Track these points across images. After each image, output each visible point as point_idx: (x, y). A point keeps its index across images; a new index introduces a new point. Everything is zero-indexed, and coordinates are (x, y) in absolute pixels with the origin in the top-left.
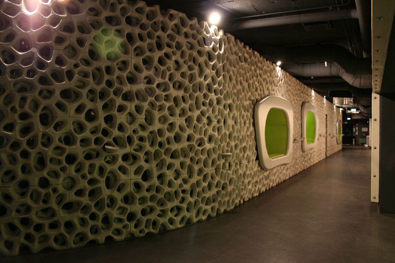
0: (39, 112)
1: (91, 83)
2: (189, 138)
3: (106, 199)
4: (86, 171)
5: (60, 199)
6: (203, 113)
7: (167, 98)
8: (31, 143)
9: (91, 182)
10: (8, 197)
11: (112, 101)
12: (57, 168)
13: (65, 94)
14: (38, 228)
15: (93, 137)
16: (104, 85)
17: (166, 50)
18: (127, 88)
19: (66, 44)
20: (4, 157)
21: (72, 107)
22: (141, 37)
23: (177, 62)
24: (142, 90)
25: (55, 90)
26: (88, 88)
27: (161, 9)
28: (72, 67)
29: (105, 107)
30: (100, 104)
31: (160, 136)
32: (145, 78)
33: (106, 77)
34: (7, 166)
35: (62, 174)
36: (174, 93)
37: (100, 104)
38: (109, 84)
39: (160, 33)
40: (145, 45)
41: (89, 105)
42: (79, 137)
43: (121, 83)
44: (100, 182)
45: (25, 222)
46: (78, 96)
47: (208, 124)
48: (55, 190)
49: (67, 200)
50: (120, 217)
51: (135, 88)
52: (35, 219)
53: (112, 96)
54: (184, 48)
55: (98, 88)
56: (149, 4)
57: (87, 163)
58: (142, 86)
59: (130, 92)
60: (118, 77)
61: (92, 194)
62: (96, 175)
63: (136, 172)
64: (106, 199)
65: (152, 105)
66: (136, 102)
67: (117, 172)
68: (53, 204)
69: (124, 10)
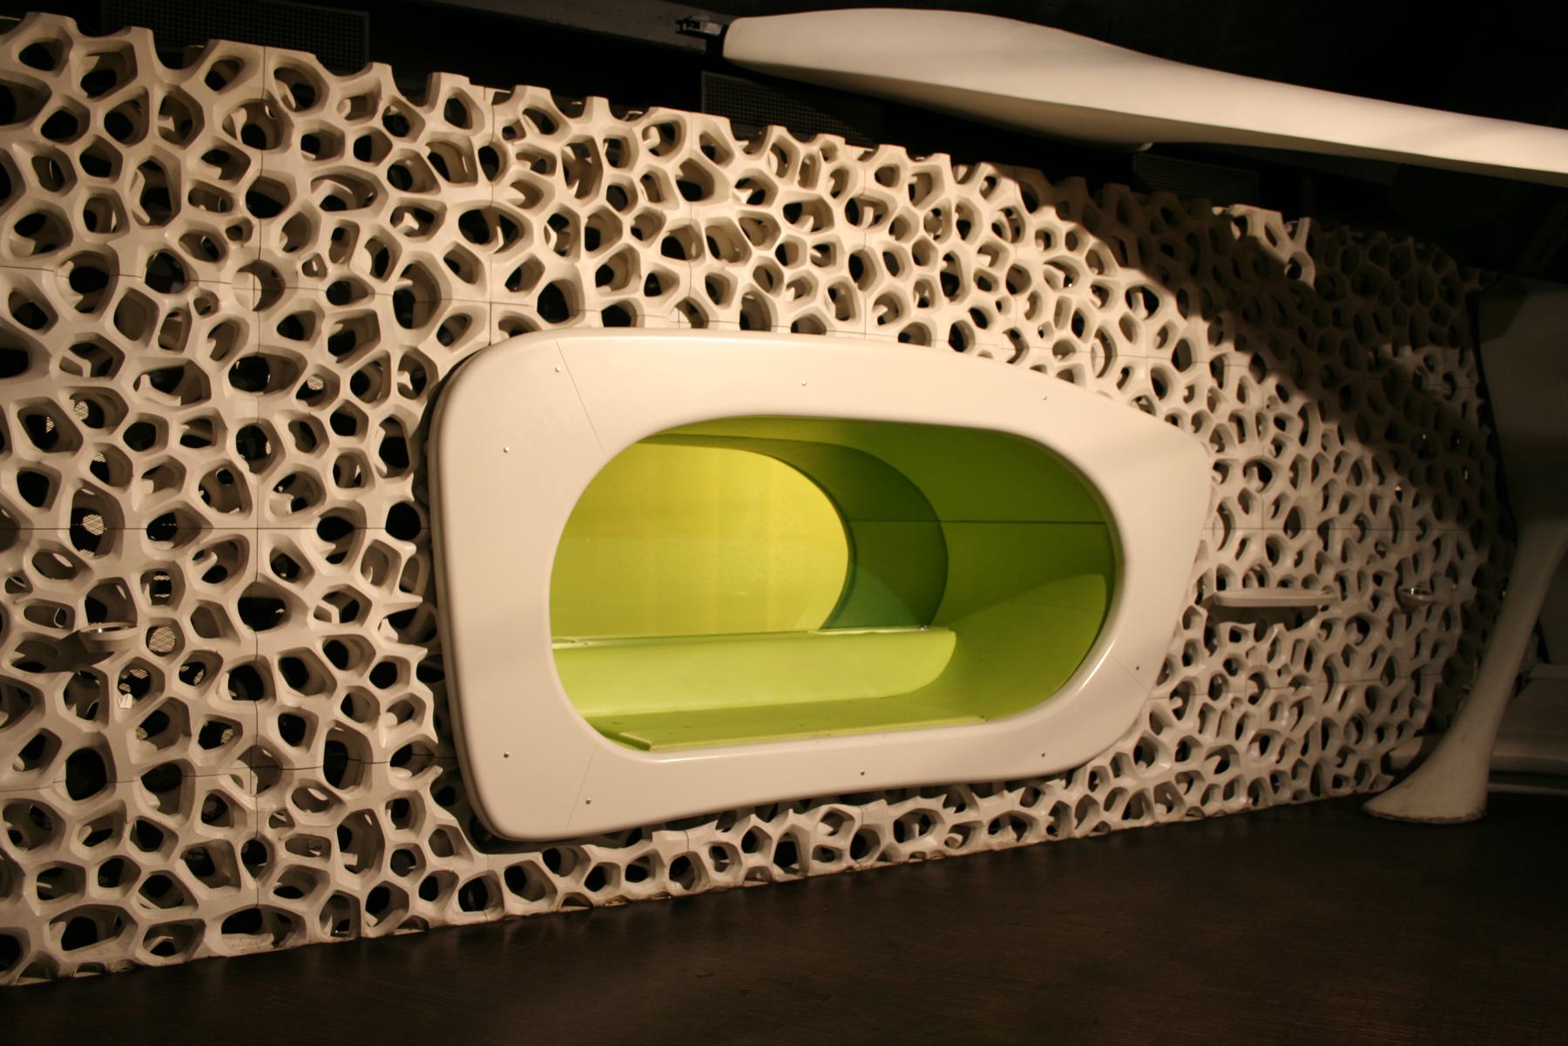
0: (395, 281)
1: (560, 193)
2: (1184, 750)
3: (395, 364)
4: (322, 244)
5: (226, 335)
6: (1231, 666)
7: (826, 252)
8: (125, 125)
9: (342, 292)
10: (34, 311)
11: (627, 257)
12: (219, 223)
13: (476, 224)
14: (146, 434)
15: (352, 133)
16: (600, 200)
17: (975, 296)
18: (678, 212)
19: (678, 295)
20: (23, 157)
21: (497, 264)
22: (893, 263)
23: (1014, 335)
24: (730, 223)
25: (444, 208)
26: (550, 210)
27: (955, 163)
28: (499, 134)
29: (604, 276)
30: (587, 264)
31: (614, 163)
32: (741, 184)
33: (610, 175)
34: (34, 195)
35: (233, 247)
36: (847, 237)
37: (587, 264)
38: (620, 197)
39: (952, 241)
40: (904, 286)
41: (554, 268)
42: (301, 123)
43: (656, 195)
44: (373, 293)
45: (102, 412)
46: (513, 231)
47: (1253, 700)
48: (207, 305)
49: (248, 348)
50: (832, 842)
51: (700, 215)
52: (143, 401)
53: (627, 239)
54: (1037, 282)
55: (584, 211)
56: (917, 150)
57: (329, 222)
58: (728, 207)
59: (687, 230)
60: (647, 179)
61: (342, 345)
62: (361, 262)
63: (516, 282)
64: (395, 364)
65: (767, 277)
66: (709, 264)
67: (439, 269)
68: (199, 349)
69: (840, 177)
